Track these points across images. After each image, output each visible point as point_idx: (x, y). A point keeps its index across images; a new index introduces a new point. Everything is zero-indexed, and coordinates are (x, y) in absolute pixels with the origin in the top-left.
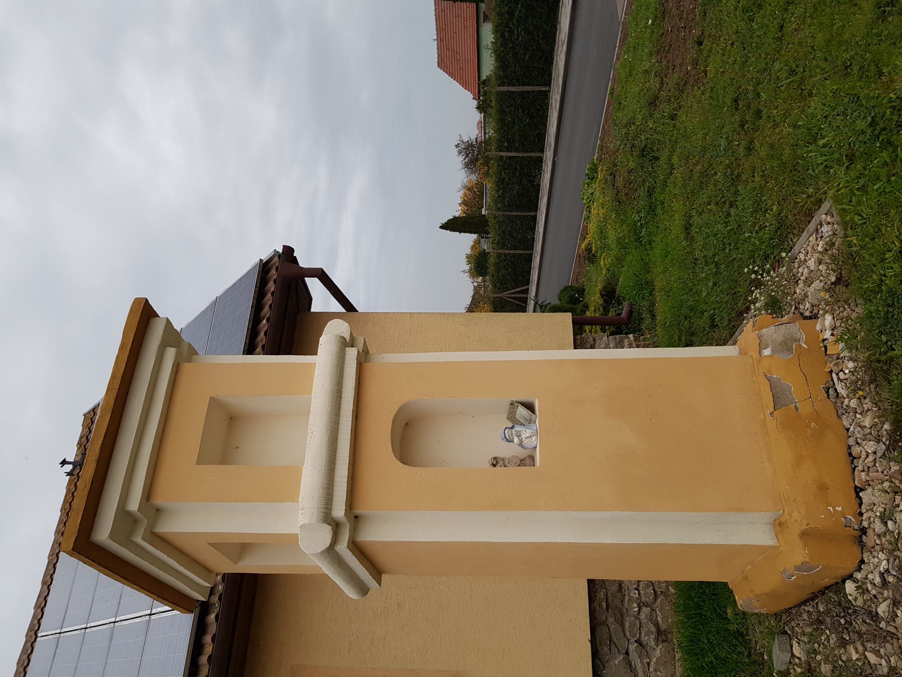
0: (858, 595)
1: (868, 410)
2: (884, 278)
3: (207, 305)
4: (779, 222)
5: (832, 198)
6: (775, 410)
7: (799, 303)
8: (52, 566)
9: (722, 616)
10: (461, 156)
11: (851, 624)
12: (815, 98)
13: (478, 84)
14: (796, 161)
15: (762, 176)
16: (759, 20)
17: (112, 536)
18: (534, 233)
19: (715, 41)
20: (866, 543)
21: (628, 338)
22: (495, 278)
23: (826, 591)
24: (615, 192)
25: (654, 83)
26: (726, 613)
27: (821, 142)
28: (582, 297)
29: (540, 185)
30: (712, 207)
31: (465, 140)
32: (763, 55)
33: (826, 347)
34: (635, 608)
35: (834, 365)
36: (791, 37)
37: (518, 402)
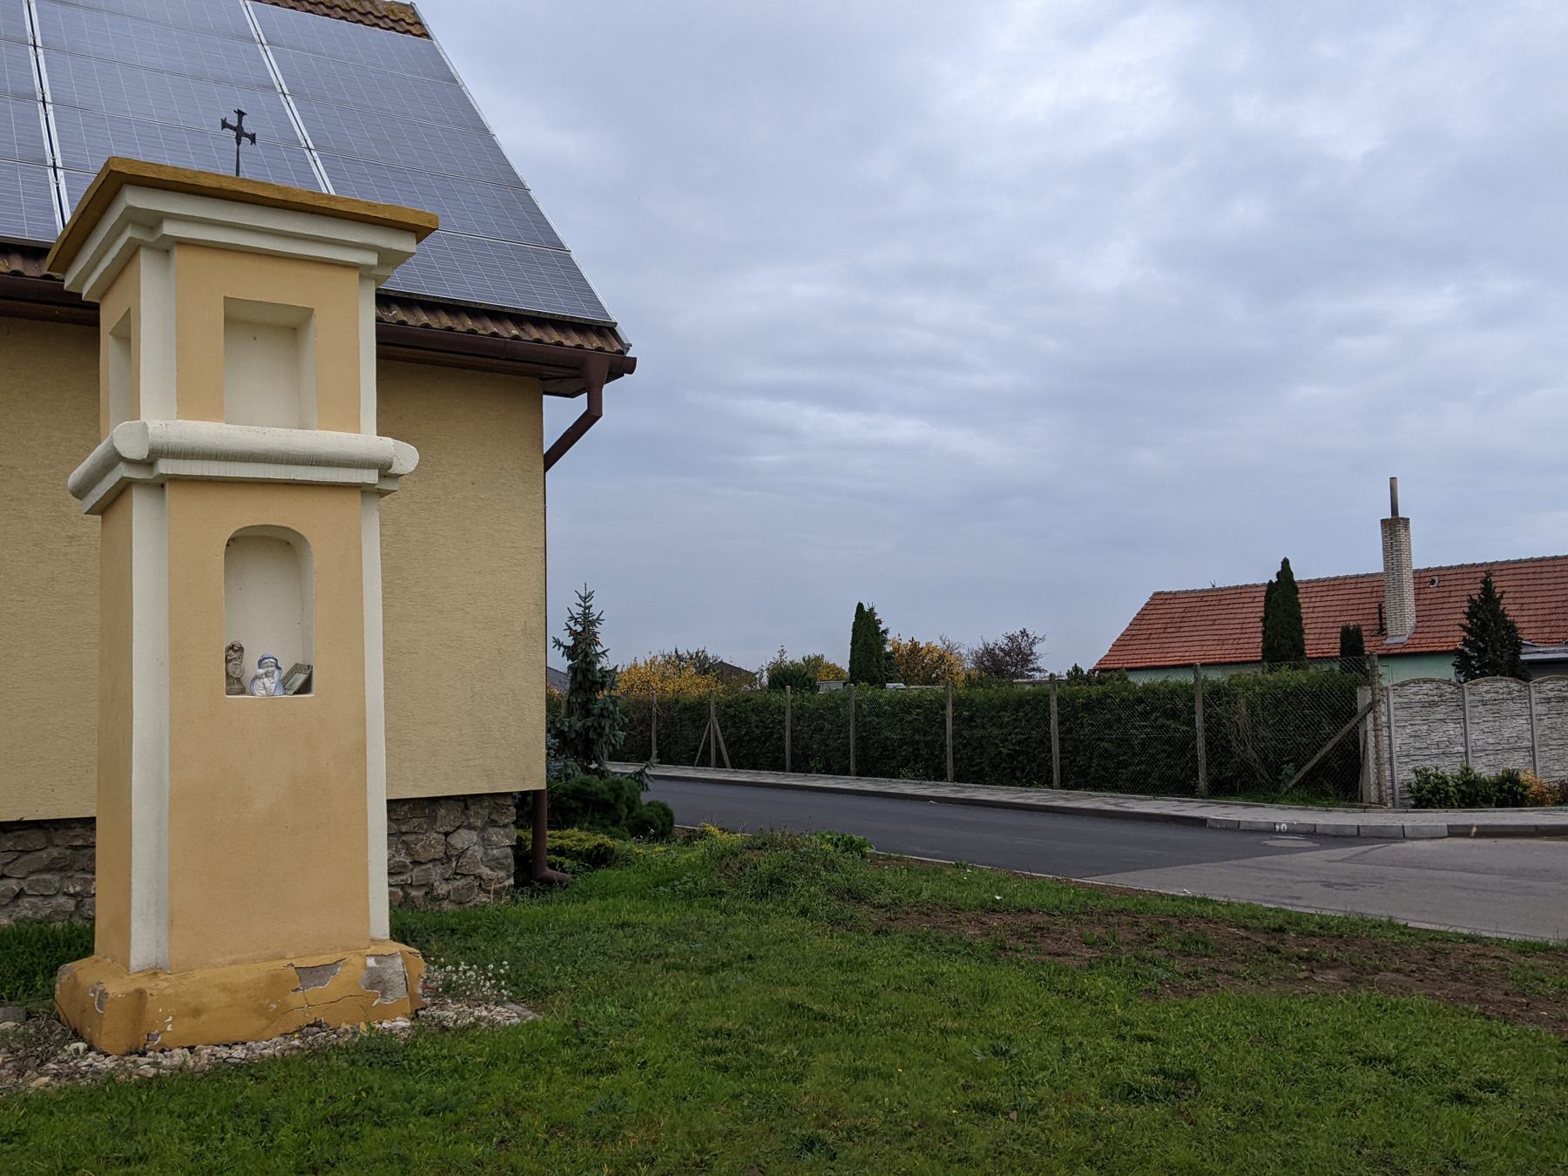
17: (129, 208)
18: (819, 772)
21: (509, 877)
22: (743, 704)
29: (899, 778)
37: (311, 674)
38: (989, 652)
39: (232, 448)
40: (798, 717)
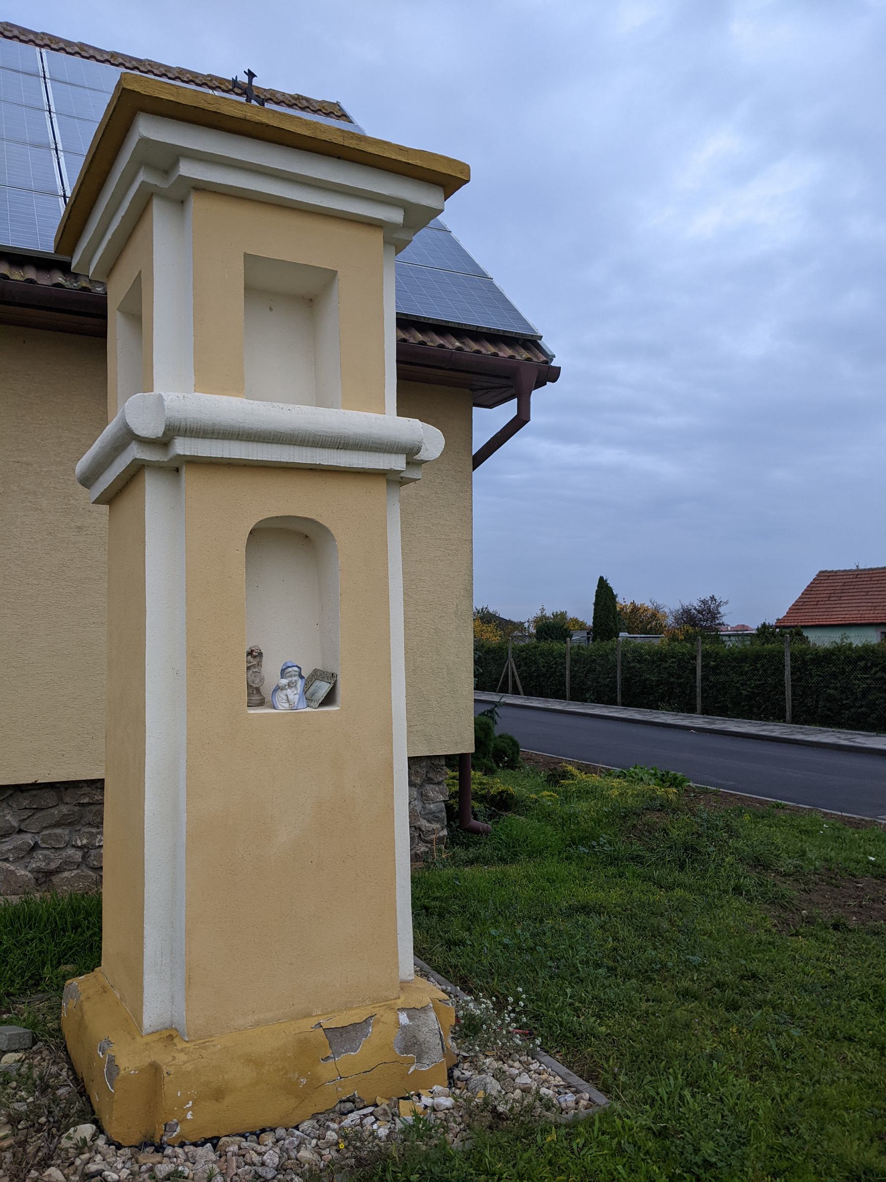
0: (74, 1141)
1: (321, 1156)
2: (496, 1178)
3: (481, 266)
4: (582, 1035)
5: (609, 1107)
6: (324, 1029)
7: (471, 1062)
8: (112, 59)
9: (63, 957)
10: (699, 604)
11: (38, 1131)
12: (748, 1084)
13: (796, 626)
14: (664, 1058)
15: (647, 1012)
16: (861, 1008)
17: (144, 141)
18: (592, 702)
19: (838, 947)
20: (144, 1152)
21: (443, 829)
22: (533, 650)
23: (84, 1098)
24: (638, 811)
25: (787, 864)
26: (66, 964)
27: (687, 1093)
28: (503, 767)
29: (658, 709)
30: (611, 944)
31: (721, 609)
32: (813, 1014)
33: (408, 1098)
34: (81, 841)
35: (384, 1110)
36: (835, 1052)
38: (686, 612)
39: (247, 426)
40: (575, 661)
